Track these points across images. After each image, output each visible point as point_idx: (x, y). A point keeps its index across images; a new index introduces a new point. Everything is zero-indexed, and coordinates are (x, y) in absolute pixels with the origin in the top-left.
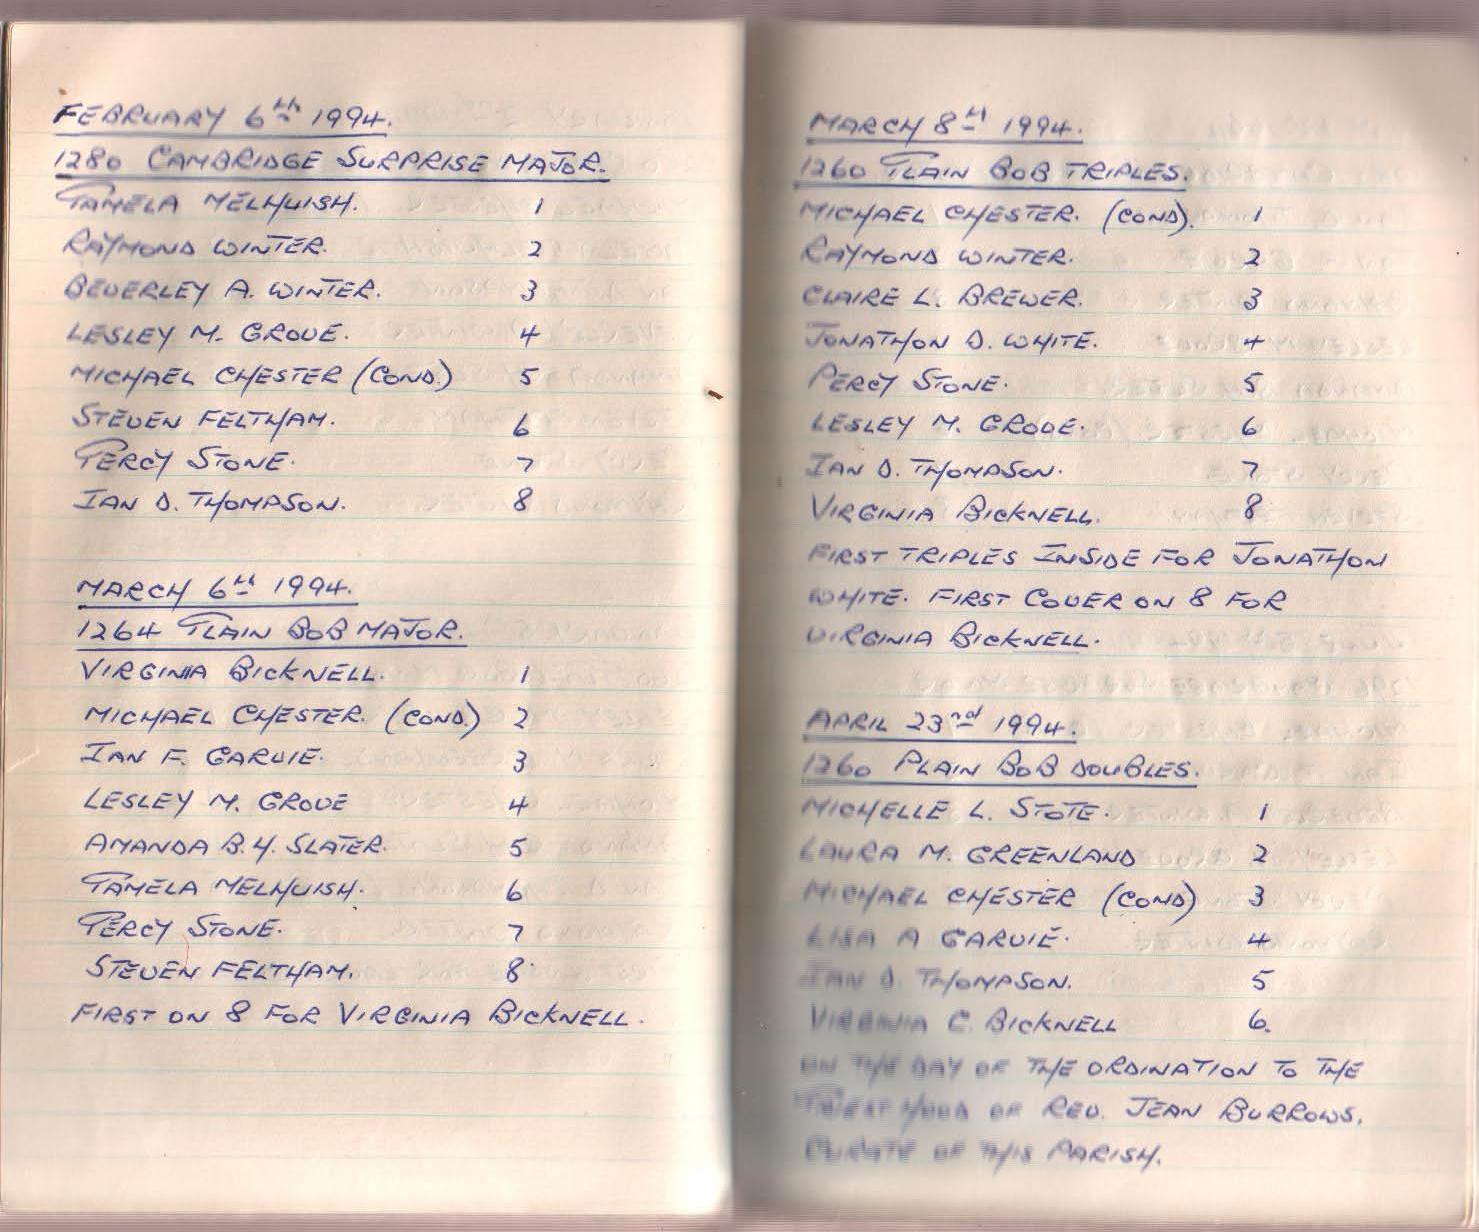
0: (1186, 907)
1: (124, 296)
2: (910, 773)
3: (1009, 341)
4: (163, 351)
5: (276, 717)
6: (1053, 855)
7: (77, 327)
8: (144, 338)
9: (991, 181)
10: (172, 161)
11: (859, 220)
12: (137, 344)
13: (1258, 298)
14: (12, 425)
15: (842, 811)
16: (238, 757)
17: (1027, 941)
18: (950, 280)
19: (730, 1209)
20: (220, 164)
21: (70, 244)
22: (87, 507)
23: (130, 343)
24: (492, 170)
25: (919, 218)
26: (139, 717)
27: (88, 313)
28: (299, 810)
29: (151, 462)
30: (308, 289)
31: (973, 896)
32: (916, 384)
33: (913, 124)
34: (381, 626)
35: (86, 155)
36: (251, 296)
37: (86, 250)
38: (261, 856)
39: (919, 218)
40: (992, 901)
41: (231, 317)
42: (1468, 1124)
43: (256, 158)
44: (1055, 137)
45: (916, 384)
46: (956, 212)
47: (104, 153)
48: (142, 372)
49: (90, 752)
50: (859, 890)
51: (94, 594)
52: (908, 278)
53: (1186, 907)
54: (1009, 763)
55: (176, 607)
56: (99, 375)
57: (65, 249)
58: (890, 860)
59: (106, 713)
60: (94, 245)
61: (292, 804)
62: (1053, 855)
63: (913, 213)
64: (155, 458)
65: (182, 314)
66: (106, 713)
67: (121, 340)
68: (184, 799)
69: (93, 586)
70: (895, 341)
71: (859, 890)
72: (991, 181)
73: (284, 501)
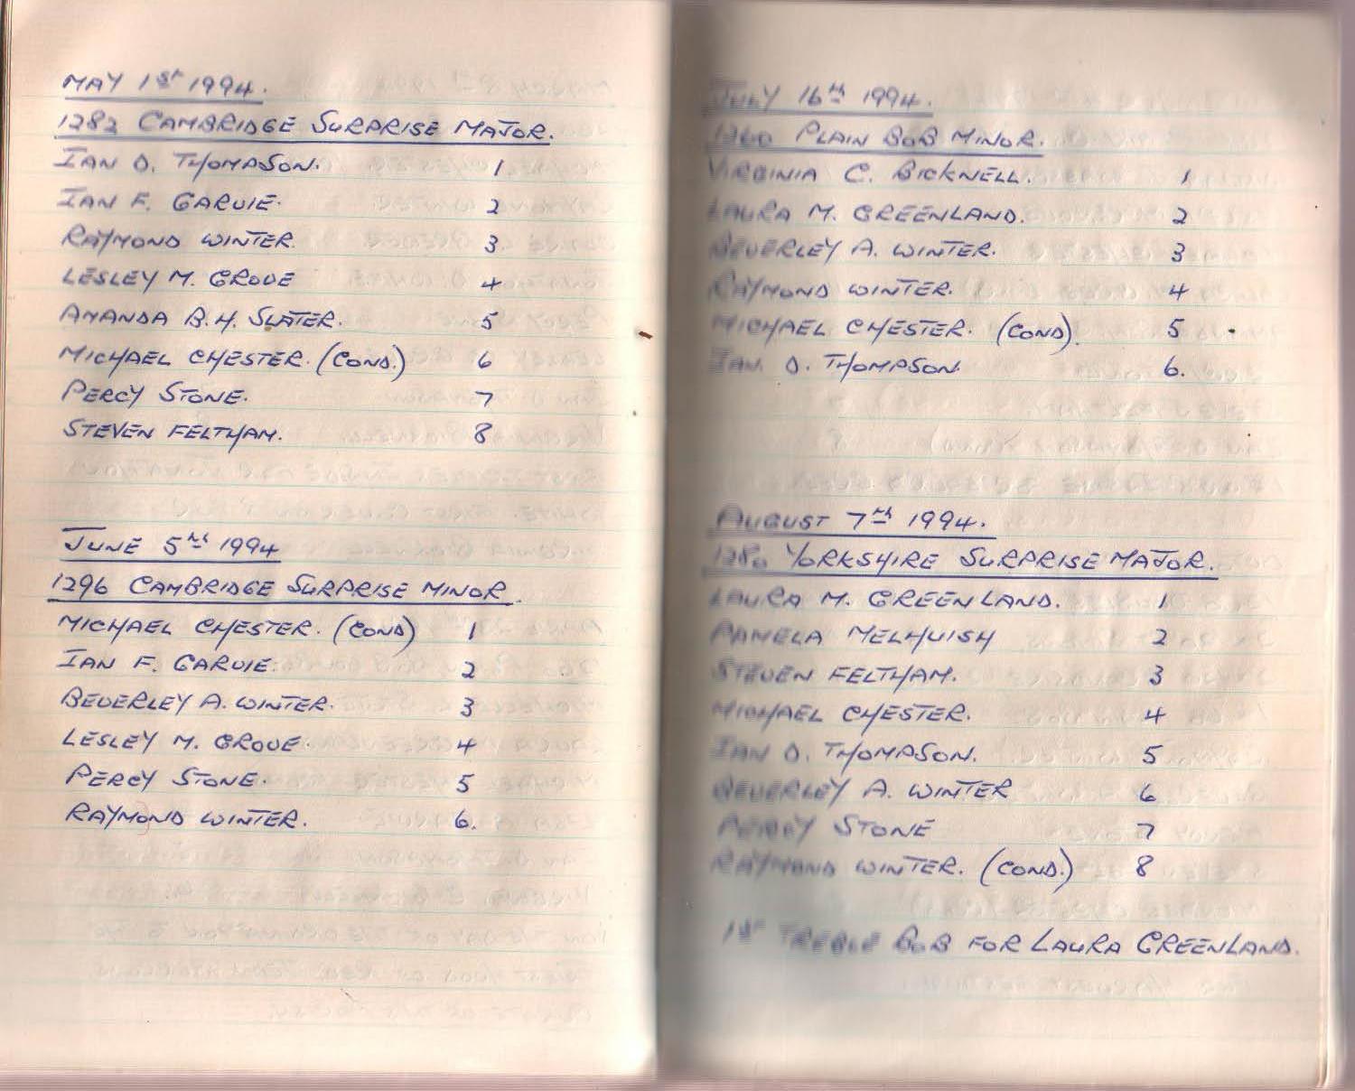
0: (1065, 339)
1: (775, 639)
2: (809, 141)
3: (898, 251)
4: (147, 293)
5: (233, 628)
6: (958, 601)
7: (70, 271)
8: (129, 280)
9: (885, 147)
10: (165, 124)
11: (768, 332)
12: (122, 286)
13: (472, 707)
14: (11, 360)
15: (749, 328)
16: (202, 663)
17: (916, 253)
18: (844, 270)
19: (654, 1071)
20: (192, 589)
21: (69, 237)
22: (65, 164)
23: (117, 284)
24: (446, 134)
25: (820, 331)
26: (107, 358)
27: (81, 259)
28: (251, 750)
29: (126, 394)
30: (280, 709)
31: (113, 625)
32: (837, 828)
33: (884, 558)
34: (878, 711)
35: (87, 119)
36: (224, 707)
37: (82, 244)
38: (214, 367)
39: (820, 331)
40: (890, 332)
41: (207, 263)
42: (1322, 994)
43: (238, 123)
44: (958, 531)
45: (837, 828)
46: (857, 325)
47: (104, 115)
48: (126, 622)
49: (66, 197)
50: (763, 323)
51: (72, 630)
52: (815, 272)
53: (1065, 339)
54: (73, 697)
55: (878, 576)
56: (86, 623)
57: (63, 242)
58: (783, 221)
59: (82, 82)
60: (90, 239)
61: (245, 744)
62: (958, 601)
63: (814, 326)
64: (177, 699)
65: (166, 261)
66: (82, 82)
67: (108, 743)
68: (149, 776)
69: (470, 127)
70: (842, 753)
71: (763, 323)
72: (885, 147)
73: (918, 751)
